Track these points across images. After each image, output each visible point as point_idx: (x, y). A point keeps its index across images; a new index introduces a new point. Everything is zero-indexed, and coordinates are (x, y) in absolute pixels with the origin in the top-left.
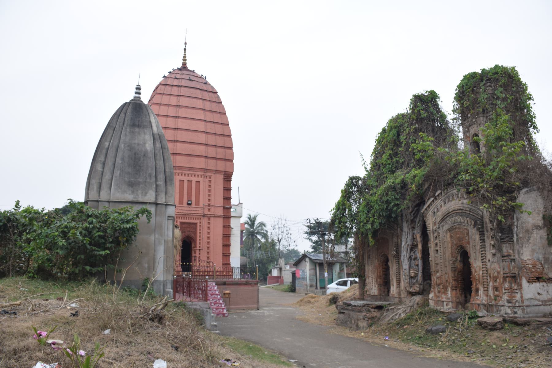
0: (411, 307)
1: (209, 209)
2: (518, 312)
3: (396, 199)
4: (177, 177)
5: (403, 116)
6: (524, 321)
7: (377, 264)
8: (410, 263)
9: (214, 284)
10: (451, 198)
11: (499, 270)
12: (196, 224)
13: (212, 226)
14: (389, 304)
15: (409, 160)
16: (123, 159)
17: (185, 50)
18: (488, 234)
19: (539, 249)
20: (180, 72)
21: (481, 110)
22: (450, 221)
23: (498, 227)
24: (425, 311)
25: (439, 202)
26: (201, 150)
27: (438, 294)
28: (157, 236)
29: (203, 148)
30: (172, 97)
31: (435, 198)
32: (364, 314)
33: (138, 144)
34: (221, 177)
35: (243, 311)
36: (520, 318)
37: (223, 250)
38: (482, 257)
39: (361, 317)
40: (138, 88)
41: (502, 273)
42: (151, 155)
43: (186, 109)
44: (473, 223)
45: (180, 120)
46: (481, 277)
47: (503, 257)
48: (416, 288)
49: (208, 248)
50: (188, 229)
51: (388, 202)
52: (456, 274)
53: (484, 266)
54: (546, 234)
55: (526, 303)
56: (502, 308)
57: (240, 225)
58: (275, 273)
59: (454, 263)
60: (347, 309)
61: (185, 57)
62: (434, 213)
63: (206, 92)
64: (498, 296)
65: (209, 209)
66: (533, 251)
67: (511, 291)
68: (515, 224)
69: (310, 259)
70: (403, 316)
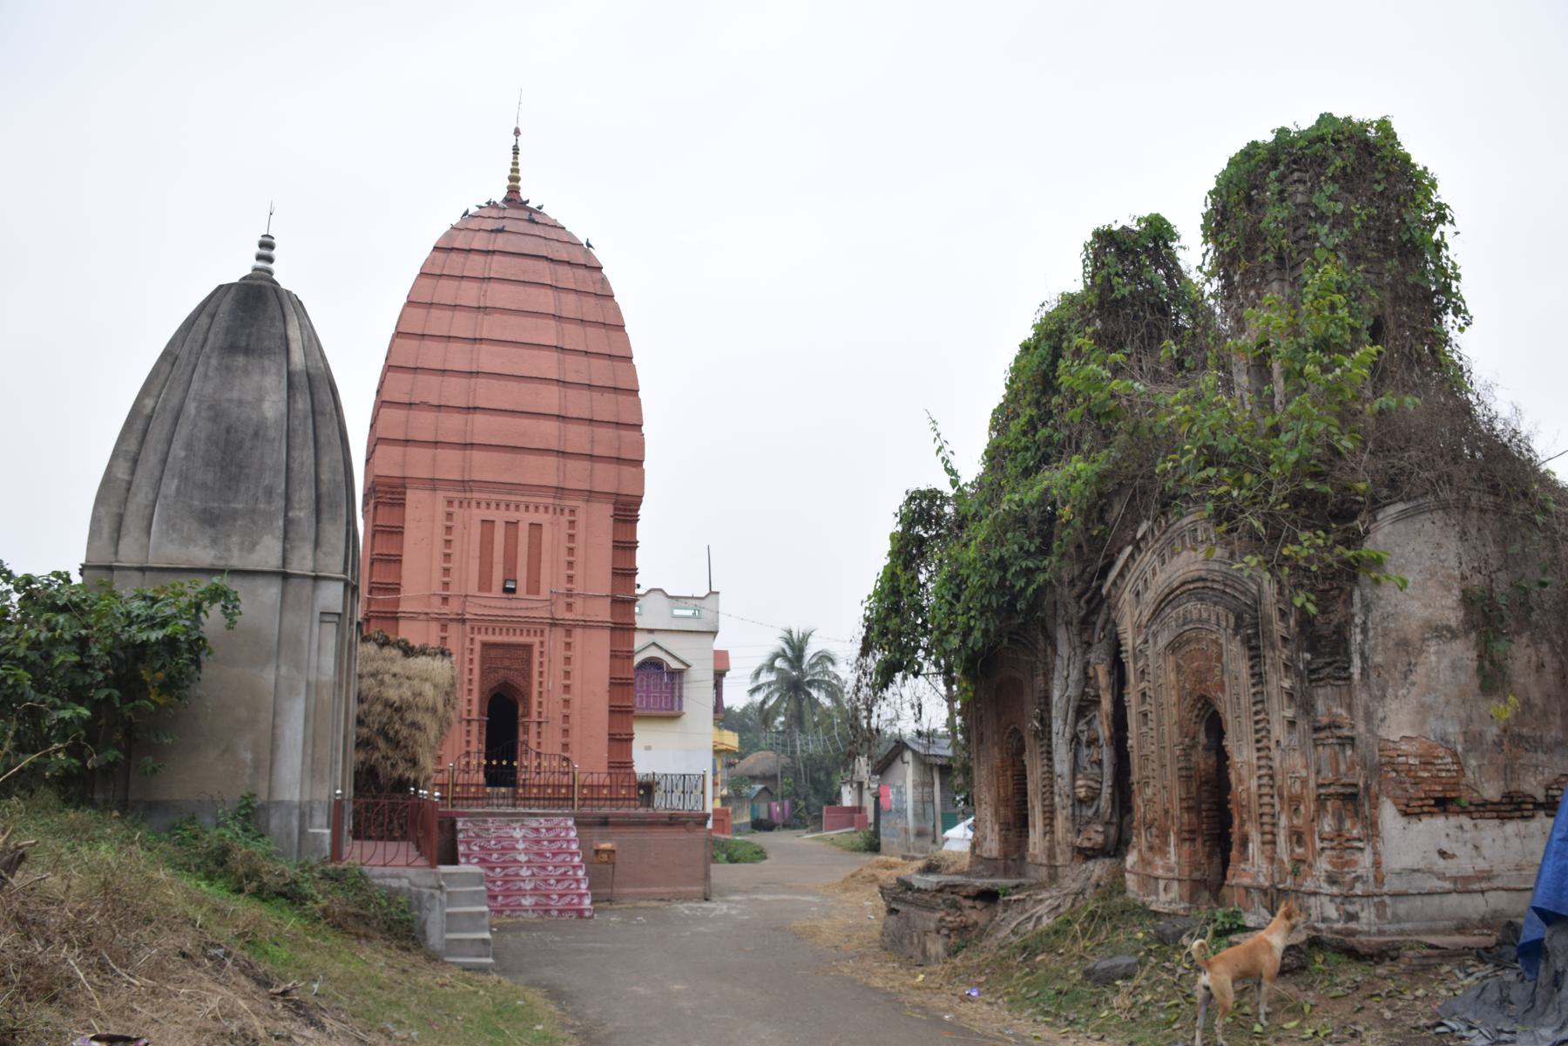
0: (1077, 894)
1: (569, 606)
2: (1362, 915)
3: (1028, 554)
4: (475, 511)
5: (1069, 300)
6: (1379, 944)
7: (997, 762)
8: (1076, 756)
9: (570, 823)
10: (1177, 542)
11: (1304, 773)
12: (528, 648)
13: (576, 654)
14: (1017, 886)
15: (1080, 433)
16: (189, 446)
17: (516, 150)
18: (1276, 656)
19: (1447, 703)
20: (494, 213)
21: (1270, 257)
22: (1171, 614)
23: (1302, 632)
24: (1113, 909)
25: (1147, 558)
26: (546, 433)
27: (1148, 855)
28: (283, 670)
29: (551, 427)
30: (465, 284)
31: (1137, 548)
32: (938, 915)
33: (240, 403)
34: (608, 510)
35: (655, 904)
36: (1368, 933)
37: (610, 726)
38: (1257, 731)
39: (932, 926)
40: (267, 244)
41: (1312, 784)
42: (276, 433)
43: (505, 317)
44: (1232, 620)
45: (484, 347)
46: (1254, 798)
47: (1317, 730)
48: (1095, 835)
49: (566, 717)
50: (507, 663)
51: (1002, 564)
52: (1194, 789)
53: (1263, 762)
54: (1474, 654)
55: (1392, 884)
56: (1312, 900)
57: (711, 655)
58: (848, 799)
59: (1187, 752)
60: (904, 901)
61: (515, 170)
62: (1138, 594)
63: (567, 268)
64: (1304, 861)
65: (569, 606)
66: (1424, 710)
67: (1342, 843)
68: (1357, 620)
69: (915, 753)
70: (1046, 921)
